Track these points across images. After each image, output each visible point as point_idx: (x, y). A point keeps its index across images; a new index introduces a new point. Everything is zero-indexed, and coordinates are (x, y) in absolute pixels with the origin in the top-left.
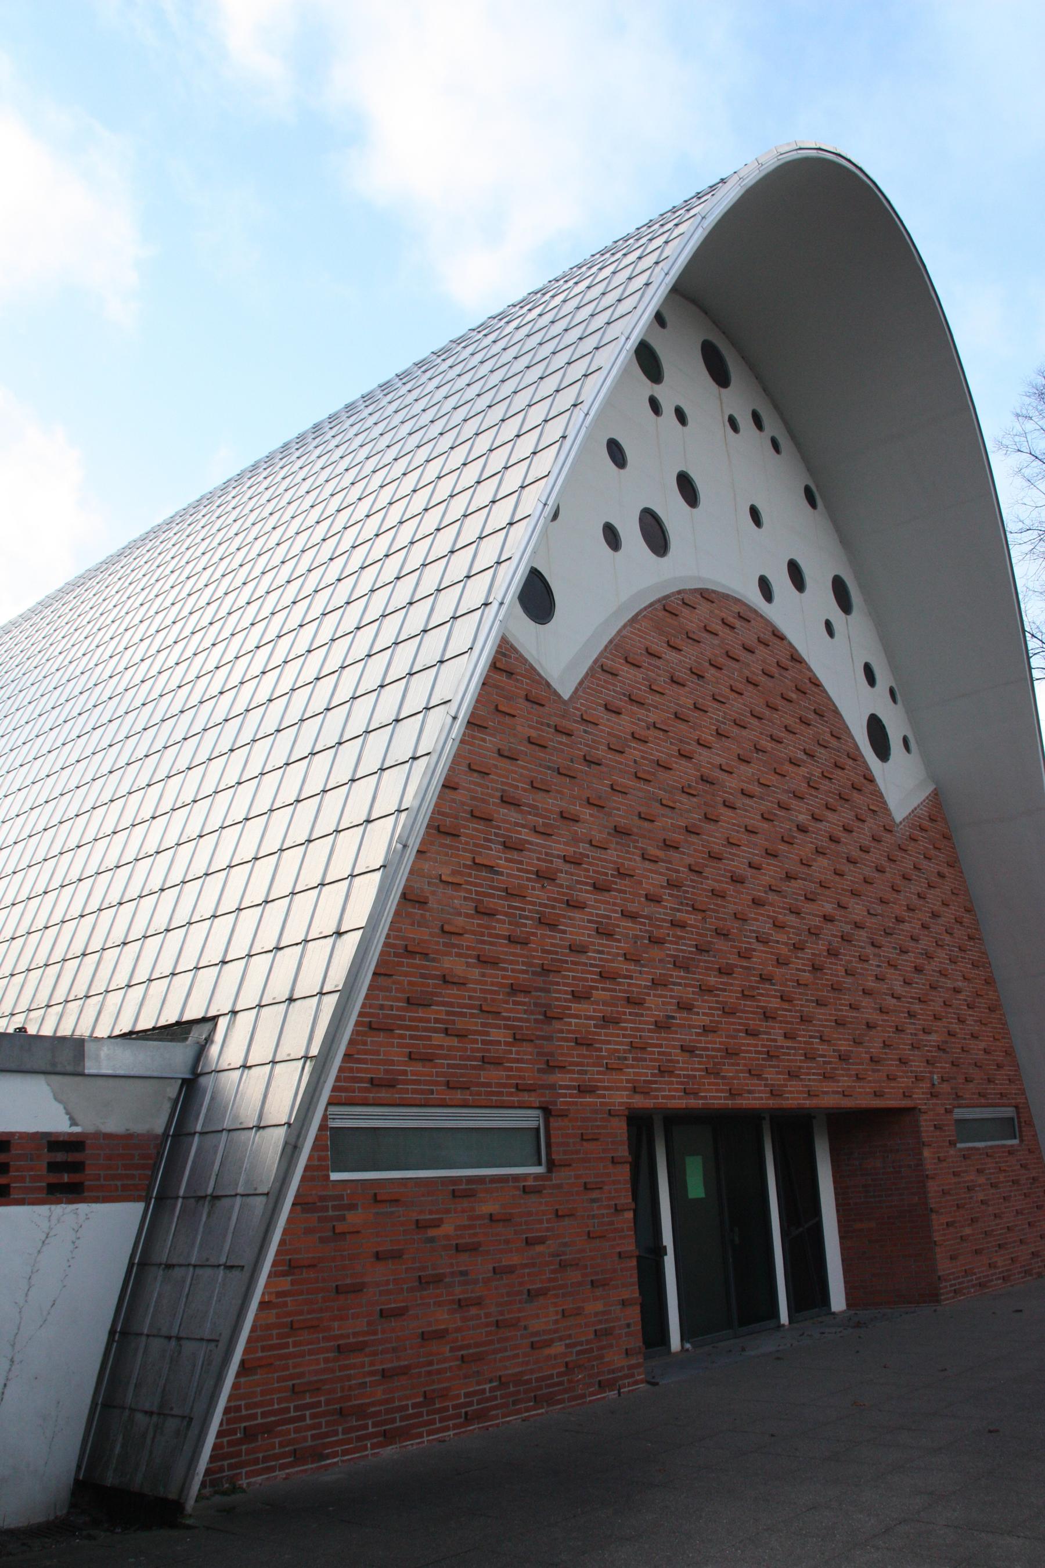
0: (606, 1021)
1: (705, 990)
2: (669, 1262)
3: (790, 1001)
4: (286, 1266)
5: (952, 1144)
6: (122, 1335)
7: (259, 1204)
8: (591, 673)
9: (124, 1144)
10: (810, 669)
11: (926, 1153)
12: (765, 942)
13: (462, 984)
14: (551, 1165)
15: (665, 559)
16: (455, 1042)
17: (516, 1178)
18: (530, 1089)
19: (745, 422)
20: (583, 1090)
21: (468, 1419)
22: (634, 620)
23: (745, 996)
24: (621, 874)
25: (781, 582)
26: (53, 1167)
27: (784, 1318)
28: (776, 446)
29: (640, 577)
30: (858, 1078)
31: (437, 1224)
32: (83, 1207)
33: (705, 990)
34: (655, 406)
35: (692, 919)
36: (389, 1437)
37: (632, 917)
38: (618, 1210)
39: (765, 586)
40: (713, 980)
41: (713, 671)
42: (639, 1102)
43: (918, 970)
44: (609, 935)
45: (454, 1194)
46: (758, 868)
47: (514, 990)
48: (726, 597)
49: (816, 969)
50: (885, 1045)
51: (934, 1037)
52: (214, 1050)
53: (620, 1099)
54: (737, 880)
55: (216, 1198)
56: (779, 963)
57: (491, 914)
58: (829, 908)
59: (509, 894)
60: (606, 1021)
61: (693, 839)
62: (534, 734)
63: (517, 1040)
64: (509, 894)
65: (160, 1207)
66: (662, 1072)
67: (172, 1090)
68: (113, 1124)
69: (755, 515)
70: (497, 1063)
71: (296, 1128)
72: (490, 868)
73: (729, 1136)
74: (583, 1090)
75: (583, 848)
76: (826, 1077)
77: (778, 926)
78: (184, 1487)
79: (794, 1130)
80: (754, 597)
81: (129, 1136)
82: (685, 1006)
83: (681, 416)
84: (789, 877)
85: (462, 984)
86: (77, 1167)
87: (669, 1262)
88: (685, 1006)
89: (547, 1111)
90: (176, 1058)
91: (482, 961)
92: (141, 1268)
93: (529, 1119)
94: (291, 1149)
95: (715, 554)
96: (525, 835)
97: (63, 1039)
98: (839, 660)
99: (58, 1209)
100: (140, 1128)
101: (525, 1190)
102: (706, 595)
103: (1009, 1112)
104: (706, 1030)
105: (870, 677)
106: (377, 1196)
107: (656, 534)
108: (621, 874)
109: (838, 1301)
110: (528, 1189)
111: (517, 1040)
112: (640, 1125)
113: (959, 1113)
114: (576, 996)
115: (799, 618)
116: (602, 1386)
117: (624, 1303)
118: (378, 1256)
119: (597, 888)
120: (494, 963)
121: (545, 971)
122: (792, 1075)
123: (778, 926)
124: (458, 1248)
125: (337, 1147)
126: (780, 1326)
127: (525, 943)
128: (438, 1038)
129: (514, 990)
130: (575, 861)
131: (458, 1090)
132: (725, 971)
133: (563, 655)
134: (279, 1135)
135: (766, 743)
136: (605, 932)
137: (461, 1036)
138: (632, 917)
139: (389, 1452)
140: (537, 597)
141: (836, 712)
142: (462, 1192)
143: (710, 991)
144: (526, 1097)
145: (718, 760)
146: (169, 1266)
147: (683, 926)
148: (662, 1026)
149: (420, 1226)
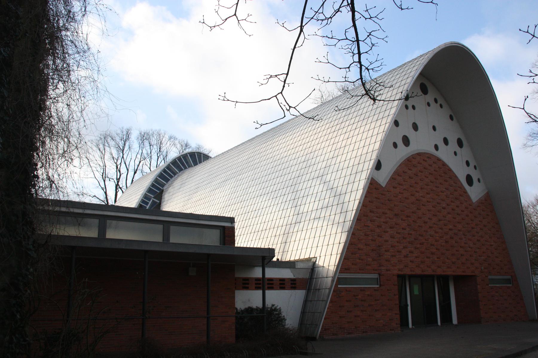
0: (392, 256)
1: (416, 248)
2: (409, 308)
3: (439, 250)
4: (331, 301)
5: (488, 285)
6: (303, 313)
7: (327, 291)
8: (390, 180)
9: (302, 280)
10: (448, 166)
11: (478, 286)
12: (432, 236)
13: (362, 250)
14: (380, 285)
15: (409, 147)
16: (361, 261)
17: (373, 287)
18: (376, 270)
19: (432, 103)
20: (387, 270)
21: (363, 332)
22: (400, 165)
23: (426, 249)
24: (396, 224)
25: (441, 145)
26: (291, 284)
27: (439, 323)
28: (441, 106)
29: (403, 152)
30: (458, 268)
31: (357, 296)
32: (296, 291)
33: (416, 248)
34: (407, 107)
35: (413, 233)
36: (349, 333)
37: (399, 233)
38: (395, 295)
39: (436, 147)
40: (418, 246)
41: (420, 173)
42: (400, 273)
43: (478, 240)
44: (393, 238)
45: (361, 290)
46: (431, 219)
47: (373, 250)
48: (425, 153)
49: (446, 242)
50: (466, 260)
51: (482, 257)
52: (317, 263)
53: (396, 272)
54: (425, 222)
55: (319, 289)
56: (436, 241)
57: (368, 235)
58: (451, 227)
59: (372, 231)
60: (392, 256)
61: (414, 214)
62: (377, 196)
63: (373, 260)
64: (372, 231)
65: (309, 291)
66: (405, 266)
67: (310, 270)
68: (300, 276)
69: (434, 128)
70: (369, 265)
71: (333, 278)
72: (368, 226)
73: (425, 280)
74: (387, 270)
75: (388, 219)
76: (448, 267)
77: (436, 232)
78: (317, 335)
79: (444, 281)
80: (432, 151)
81: (303, 279)
82: (411, 252)
83: (414, 107)
84: (440, 220)
85: (362, 250)
86: (284, 284)
87: (409, 308)
88: (411, 252)
89: (379, 274)
90: (311, 264)
91: (366, 245)
92: (306, 302)
93: (376, 276)
94: (333, 281)
95: (423, 142)
96: (375, 218)
97: (287, 262)
98: (457, 164)
99: (293, 291)
100: (305, 277)
101: (375, 290)
102: (419, 154)
103: (509, 277)
104: (416, 257)
105: (468, 163)
106: (346, 289)
107: (406, 141)
108: (396, 224)
109: (455, 321)
110: (375, 290)
111: (373, 260)
112: (402, 278)
113: (490, 277)
114: (386, 251)
115: (445, 154)
116: (391, 330)
117: (396, 314)
118: (347, 301)
119: (391, 228)
120: (369, 245)
121: (379, 246)
122: (439, 267)
123: (436, 232)
124: (362, 300)
125: (340, 281)
126: (438, 325)
127: (375, 241)
128: (358, 260)
129: (373, 250)
130: (386, 223)
131: (362, 270)
132: (422, 244)
133: (383, 178)
134: (330, 279)
135: (435, 189)
136: (392, 237)
137: (362, 260)
138: (399, 233)
139: (348, 336)
140: (378, 166)
141: (456, 176)
142: (362, 290)
143: (418, 248)
144: (375, 272)
145: (421, 195)
146: (311, 301)
147: (411, 234)
148: (406, 256)
149: (354, 296)
